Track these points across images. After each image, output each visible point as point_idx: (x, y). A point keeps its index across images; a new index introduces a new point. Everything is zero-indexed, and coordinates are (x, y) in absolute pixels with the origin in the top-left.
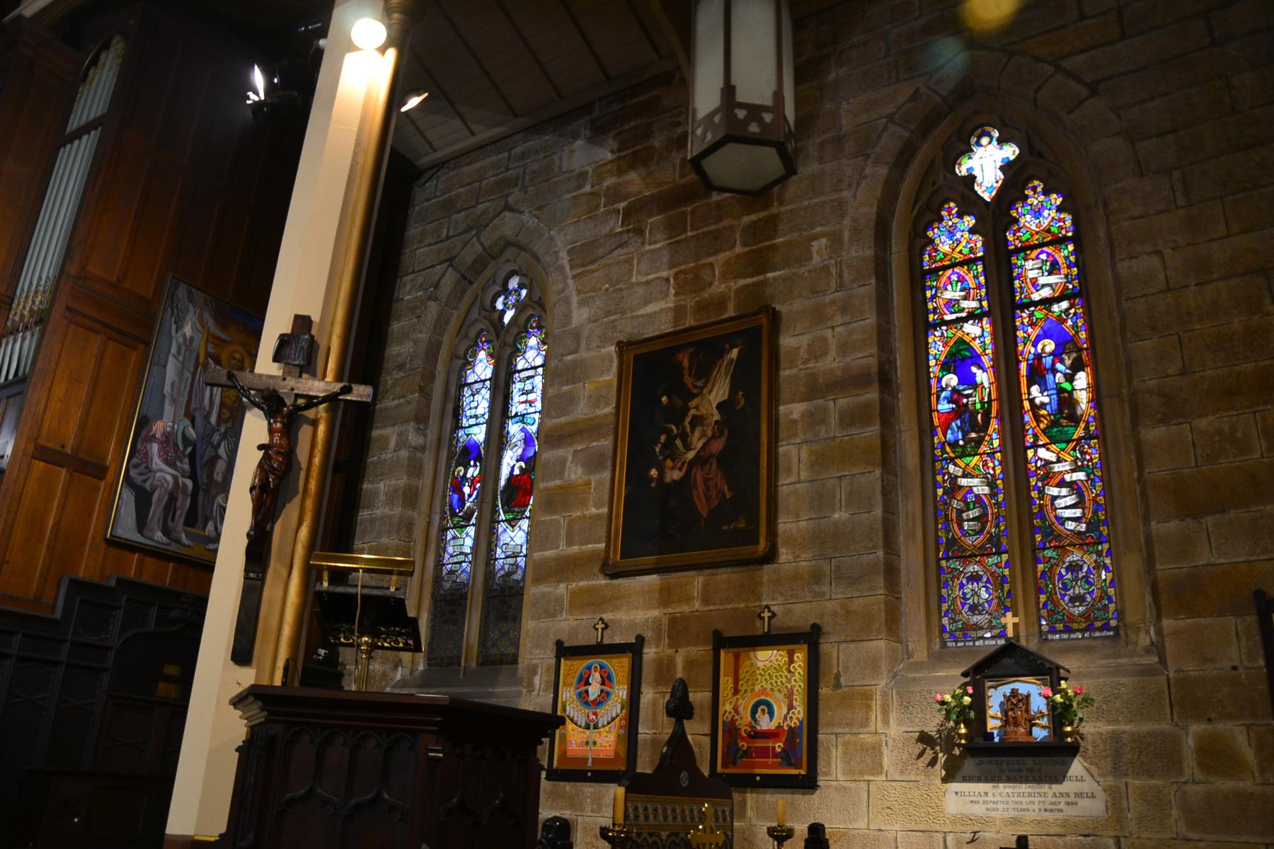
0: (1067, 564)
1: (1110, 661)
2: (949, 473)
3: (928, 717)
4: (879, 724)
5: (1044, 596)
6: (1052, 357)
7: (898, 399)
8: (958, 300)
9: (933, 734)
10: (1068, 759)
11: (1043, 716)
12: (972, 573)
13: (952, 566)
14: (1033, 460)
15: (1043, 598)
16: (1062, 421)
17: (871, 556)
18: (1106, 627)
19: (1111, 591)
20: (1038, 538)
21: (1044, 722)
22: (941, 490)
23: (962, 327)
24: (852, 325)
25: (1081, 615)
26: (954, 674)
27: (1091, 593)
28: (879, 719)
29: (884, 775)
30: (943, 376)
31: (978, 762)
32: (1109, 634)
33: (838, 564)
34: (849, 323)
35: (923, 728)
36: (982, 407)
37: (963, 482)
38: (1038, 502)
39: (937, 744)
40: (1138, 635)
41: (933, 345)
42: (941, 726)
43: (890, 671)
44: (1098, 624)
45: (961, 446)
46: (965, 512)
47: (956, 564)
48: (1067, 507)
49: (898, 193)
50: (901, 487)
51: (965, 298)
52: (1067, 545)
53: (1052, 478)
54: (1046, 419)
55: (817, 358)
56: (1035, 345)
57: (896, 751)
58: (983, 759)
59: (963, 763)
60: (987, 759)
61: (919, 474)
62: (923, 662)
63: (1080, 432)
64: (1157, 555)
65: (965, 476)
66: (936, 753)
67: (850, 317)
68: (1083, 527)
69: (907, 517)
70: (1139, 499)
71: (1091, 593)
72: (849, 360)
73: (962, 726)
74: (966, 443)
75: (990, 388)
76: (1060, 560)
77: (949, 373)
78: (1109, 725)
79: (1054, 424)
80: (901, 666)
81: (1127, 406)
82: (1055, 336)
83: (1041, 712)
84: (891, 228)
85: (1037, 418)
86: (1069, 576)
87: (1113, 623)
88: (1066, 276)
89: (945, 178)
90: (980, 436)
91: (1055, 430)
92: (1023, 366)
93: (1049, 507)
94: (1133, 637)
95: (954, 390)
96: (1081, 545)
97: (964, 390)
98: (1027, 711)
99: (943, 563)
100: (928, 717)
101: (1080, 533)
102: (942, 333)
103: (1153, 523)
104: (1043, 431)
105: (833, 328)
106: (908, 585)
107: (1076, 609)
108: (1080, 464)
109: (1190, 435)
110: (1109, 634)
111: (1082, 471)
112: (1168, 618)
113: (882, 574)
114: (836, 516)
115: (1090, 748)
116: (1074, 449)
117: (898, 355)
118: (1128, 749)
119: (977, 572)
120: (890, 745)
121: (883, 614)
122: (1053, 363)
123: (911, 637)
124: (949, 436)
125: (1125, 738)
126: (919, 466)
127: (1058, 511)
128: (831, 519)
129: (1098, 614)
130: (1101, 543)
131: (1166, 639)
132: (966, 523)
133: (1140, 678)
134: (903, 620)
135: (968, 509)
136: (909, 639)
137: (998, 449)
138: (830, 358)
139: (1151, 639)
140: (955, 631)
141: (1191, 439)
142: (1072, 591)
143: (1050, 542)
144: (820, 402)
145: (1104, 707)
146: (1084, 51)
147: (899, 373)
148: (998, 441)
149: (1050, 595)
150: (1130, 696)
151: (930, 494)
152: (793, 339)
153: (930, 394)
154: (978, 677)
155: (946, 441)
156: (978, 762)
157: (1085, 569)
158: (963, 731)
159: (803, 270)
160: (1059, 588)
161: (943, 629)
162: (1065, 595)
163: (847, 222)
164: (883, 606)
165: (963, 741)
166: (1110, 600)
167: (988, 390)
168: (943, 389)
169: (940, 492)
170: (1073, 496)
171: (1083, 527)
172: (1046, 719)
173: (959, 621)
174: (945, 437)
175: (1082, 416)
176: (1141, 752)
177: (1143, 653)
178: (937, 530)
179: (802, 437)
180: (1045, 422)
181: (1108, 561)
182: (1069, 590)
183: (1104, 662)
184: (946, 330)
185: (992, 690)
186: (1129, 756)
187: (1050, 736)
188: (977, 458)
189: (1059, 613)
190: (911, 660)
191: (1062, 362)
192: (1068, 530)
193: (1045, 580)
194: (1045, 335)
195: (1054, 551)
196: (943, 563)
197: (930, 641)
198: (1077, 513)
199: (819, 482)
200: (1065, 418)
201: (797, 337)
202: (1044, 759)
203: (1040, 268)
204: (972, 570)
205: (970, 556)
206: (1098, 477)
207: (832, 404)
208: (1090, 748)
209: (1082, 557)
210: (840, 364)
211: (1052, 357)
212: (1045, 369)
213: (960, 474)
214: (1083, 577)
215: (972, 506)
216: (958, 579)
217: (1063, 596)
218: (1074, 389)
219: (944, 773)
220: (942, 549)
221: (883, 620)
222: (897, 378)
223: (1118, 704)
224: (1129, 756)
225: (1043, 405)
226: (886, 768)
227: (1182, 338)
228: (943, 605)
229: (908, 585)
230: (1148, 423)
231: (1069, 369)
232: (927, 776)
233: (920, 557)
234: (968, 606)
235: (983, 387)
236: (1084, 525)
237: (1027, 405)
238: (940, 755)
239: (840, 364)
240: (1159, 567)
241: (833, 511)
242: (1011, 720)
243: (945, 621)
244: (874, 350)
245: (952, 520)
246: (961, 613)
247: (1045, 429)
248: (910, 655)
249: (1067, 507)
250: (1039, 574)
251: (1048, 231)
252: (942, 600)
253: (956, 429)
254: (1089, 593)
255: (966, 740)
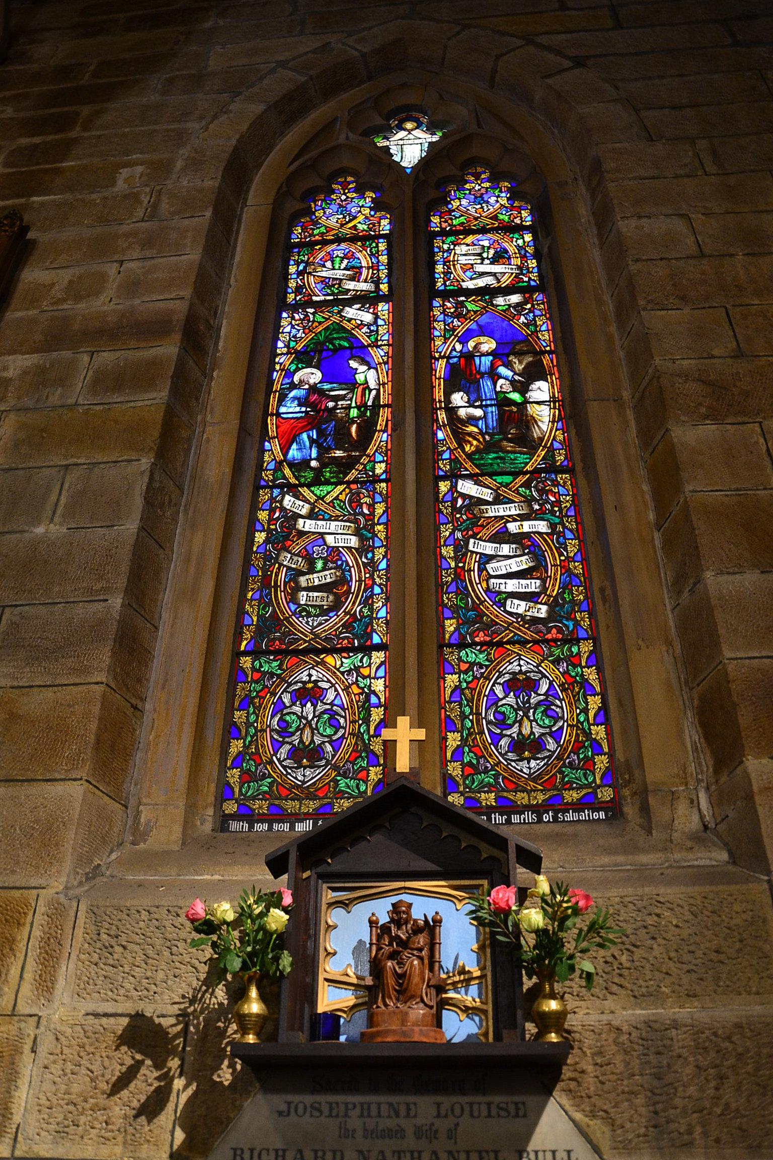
0: (507, 677)
1: (621, 859)
2: (283, 509)
3: (161, 975)
4: (27, 989)
5: (457, 736)
6: (491, 358)
7: (212, 378)
8: (341, 280)
9: (166, 1022)
10: (531, 1100)
11: (467, 982)
12: (304, 683)
13: (266, 668)
14: (448, 498)
15: (453, 740)
16: (505, 443)
17: (100, 606)
18: (588, 802)
19: (599, 732)
20: (450, 626)
21: (470, 996)
22: (264, 535)
23: (342, 310)
24: (156, 261)
25: (534, 778)
26: (240, 878)
27: (557, 735)
28: (28, 976)
29: (8, 1139)
30: (297, 369)
31: (283, 1107)
32: (595, 816)
33: (17, 619)
34: (153, 258)
35: (141, 1006)
36: (362, 415)
37: (308, 525)
38: (453, 564)
39: (173, 1052)
40: (673, 809)
41: (288, 329)
42: (192, 1001)
43: (82, 860)
44: (571, 796)
45: (312, 469)
46: (304, 574)
47: (271, 665)
48: (510, 576)
49: (271, 148)
50: (186, 511)
51: (352, 279)
52: (508, 642)
53: (483, 526)
54: (475, 439)
55: (78, 298)
56: (463, 340)
57: (56, 1069)
58: (295, 1098)
59: (240, 1108)
60: (308, 1099)
61: (226, 490)
62: (167, 853)
63: (537, 461)
64: (722, 631)
65: (312, 515)
66: (167, 1079)
67: (155, 251)
68: (542, 611)
69: (188, 560)
70: (660, 553)
71: (557, 735)
72: (137, 301)
73: (254, 993)
74: (323, 465)
75: (378, 391)
76: (493, 665)
77: (309, 366)
78: (638, 1006)
79: (490, 447)
80: (114, 856)
81: (630, 414)
82: (498, 335)
83: (463, 971)
84: (252, 181)
85: (460, 437)
86: (511, 700)
87: (606, 794)
88: (520, 268)
89: (347, 138)
90: (349, 456)
91: (493, 455)
92: (441, 366)
93: (475, 575)
94: (660, 811)
95: (313, 389)
96: (536, 642)
97: (332, 390)
98: (432, 962)
99: (246, 662)
100: (161, 975)
101: (535, 620)
102: (307, 316)
103: (709, 575)
104: (469, 456)
105: (121, 263)
106: (163, 688)
107: (524, 764)
108: (536, 507)
109: (762, 440)
110: (595, 816)
111: (542, 519)
112: (758, 756)
113: (110, 643)
114: (40, 530)
115: (590, 1068)
116: (527, 485)
117: (225, 322)
118: (690, 1070)
119: (316, 682)
120: (42, 1049)
121: (93, 726)
122: (493, 367)
123: (149, 795)
124: (294, 453)
125: (681, 1039)
126: (228, 479)
127: (492, 581)
128: (26, 535)
129: (571, 775)
130: (578, 641)
131: (758, 799)
132: (305, 593)
133: (707, 888)
134: (139, 755)
135: (312, 570)
136: (144, 800)
137: (384, 477)
138: (103, 298)
139: (702, 817)
140: (254, 798)
141: (764, 448)
142: (515, 729)
143: (472, 635)
144: (66, 354)
145: (624, 958)
146: (565, 33)
147: (221, 344)
148: (383, 465)
149: (469, 734)
150: (685, 933)
151: (241, 532)
152: (47, 272)
153: (269, 391)
154: (305, 875)
155: (285, 460)
156: (283, 1107)
157: (544, 687)
158: (254, 1006)
159: (94, 196)
160: (489, 722)
161: (225, 793)
162: (502, 736)
163: (185, 151)
164: (96, 709)
165: (251, 1039)
166: (597, 747)
167: (374, 393)
168: (293, 386)
169: (260, 537)
170: (524, 558)
171: (542, 611)
172: (474, 989)
173: (264, 777)
174: (285, 454)
175: (542, 439)
176: (722, 1078)
177: (689, 844)
178: (242, 599)
179: (12, 402)
180: (475, 443)
181: (591, 675)
182: (510, 727)
183: (606, 860)
184: (313, 314)
185: (339, 912)
186: (692, 1090)
187: (486, 1034)
188: (341, 488)
189: (486, 771)
190: (142, 845)
191: (509, 365)
192: (511, 614)
193: (461, 705)
194: (483, 331)
195: (481, 652)
196: (246, 662)
197: (191, 809)
198: (533, 585)
199: (21, 472)
200: (510, 440)
201: (53, 271)
202: (464, 1100)
203: (480, 255)
204: (306, 679)
205: (306, 652)
206: (571, 530)
207: (86, 358)
208: (590, 1068)
209: (539, 665)
210: (119, 307)
211: (491, 358)
212: (479, 372)
213: (304, 512)
214: (539, 704)
215: (319, 565)
216: (274, 694)
217: (496, 739)
218: (526, 402)
219: (180, 1136)
220: (247, 635)
221: (92, 738)
222: (217, 350)
223: (656, 952)
224: (692, 1090)
225: (472, 420)
226: (17, 1118)
227: (730, 313)
228: (234, 743)
229: (163, 688)
230: (683, 418)
231: (519, 375)
232: (132, 1143)
233: (201, 633)
234: (287, 747)
235: (368, 387)
236: (544, 608)
237: (442, 416)
238: (179, 1083)
239: (119, 307)
240: (728, 654)
241: (37, 522)
242: (391, 981)
243: (234, 775)
244: (187, 293)
245: (276, 586)
246: (271, 762)
247: (473, 453)
248: (139, 835)
249: (510, 576)
250: (448, 691)
251: (495, 218)
252: (232, 731)
253: (308, 444)
254: (552, 734)
255: (258, 1035)
